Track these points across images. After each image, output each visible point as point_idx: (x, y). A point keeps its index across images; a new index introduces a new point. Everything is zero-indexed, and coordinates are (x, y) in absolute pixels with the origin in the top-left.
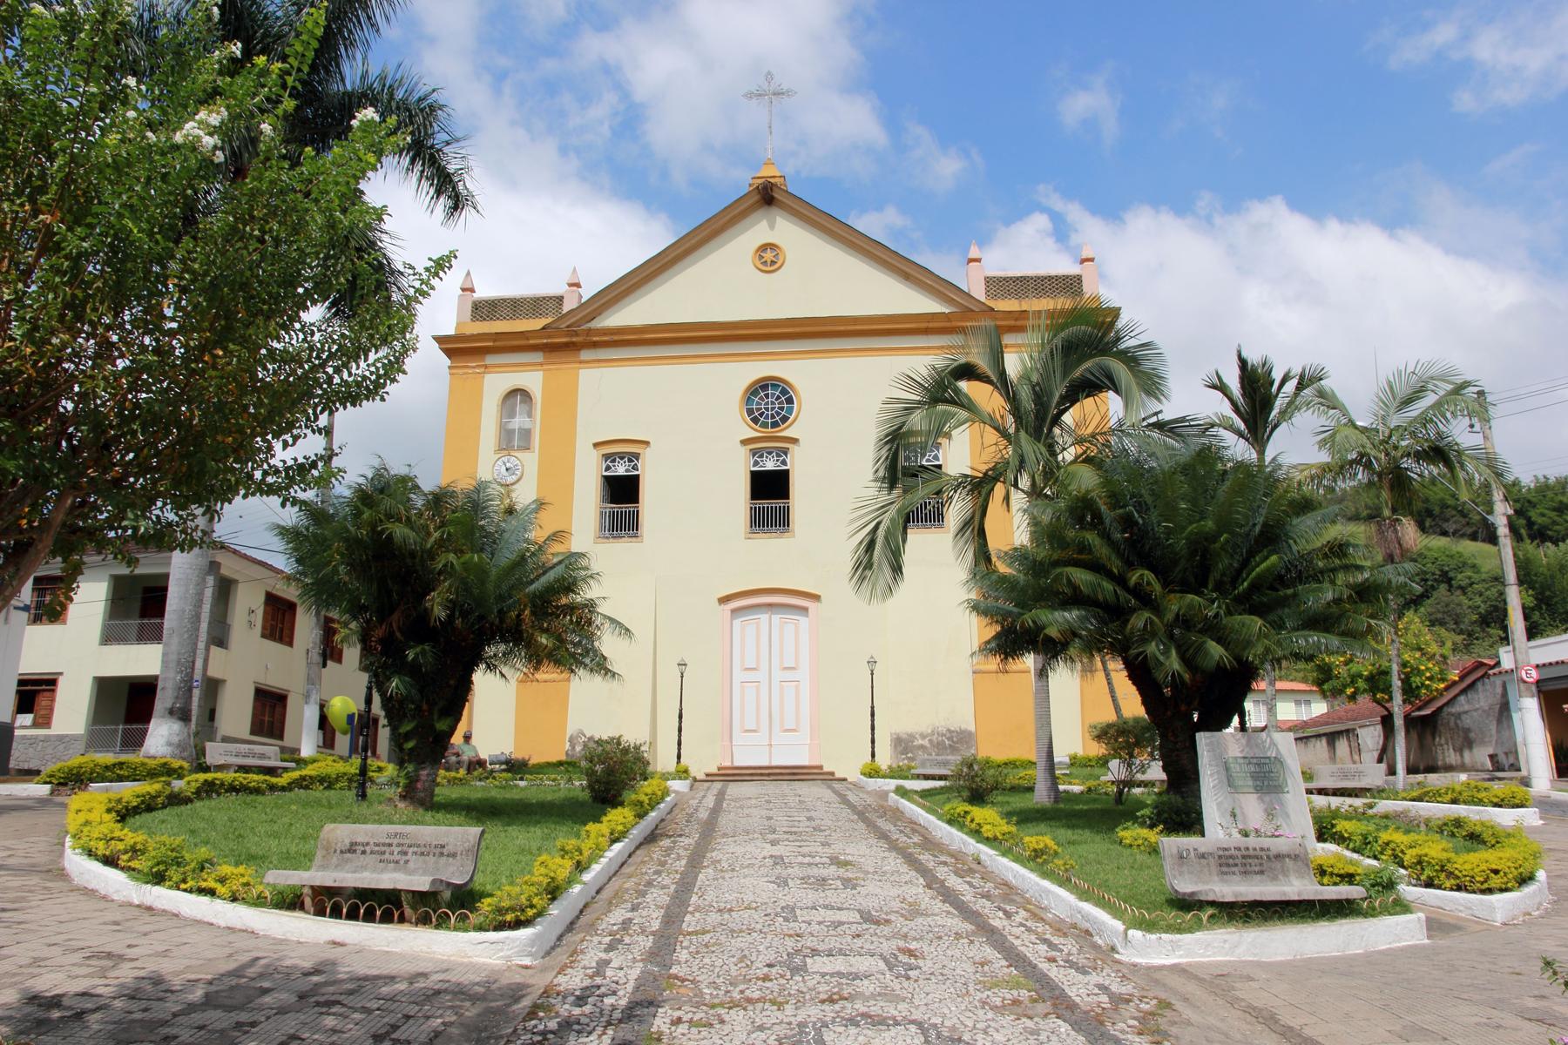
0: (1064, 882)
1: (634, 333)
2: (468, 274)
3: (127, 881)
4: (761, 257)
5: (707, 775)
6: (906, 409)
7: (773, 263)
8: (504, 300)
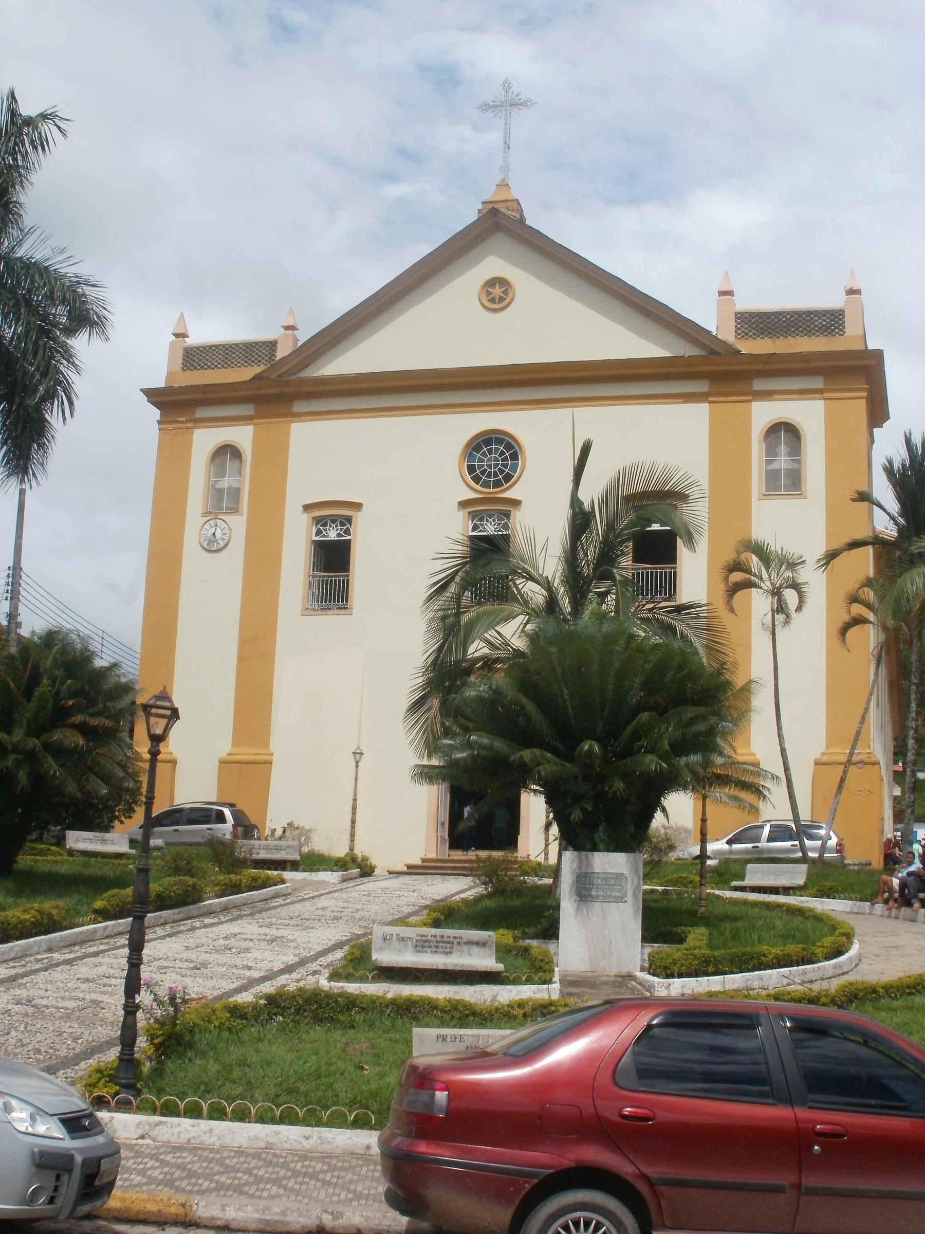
4: (489, 293)
8: (217, 346)
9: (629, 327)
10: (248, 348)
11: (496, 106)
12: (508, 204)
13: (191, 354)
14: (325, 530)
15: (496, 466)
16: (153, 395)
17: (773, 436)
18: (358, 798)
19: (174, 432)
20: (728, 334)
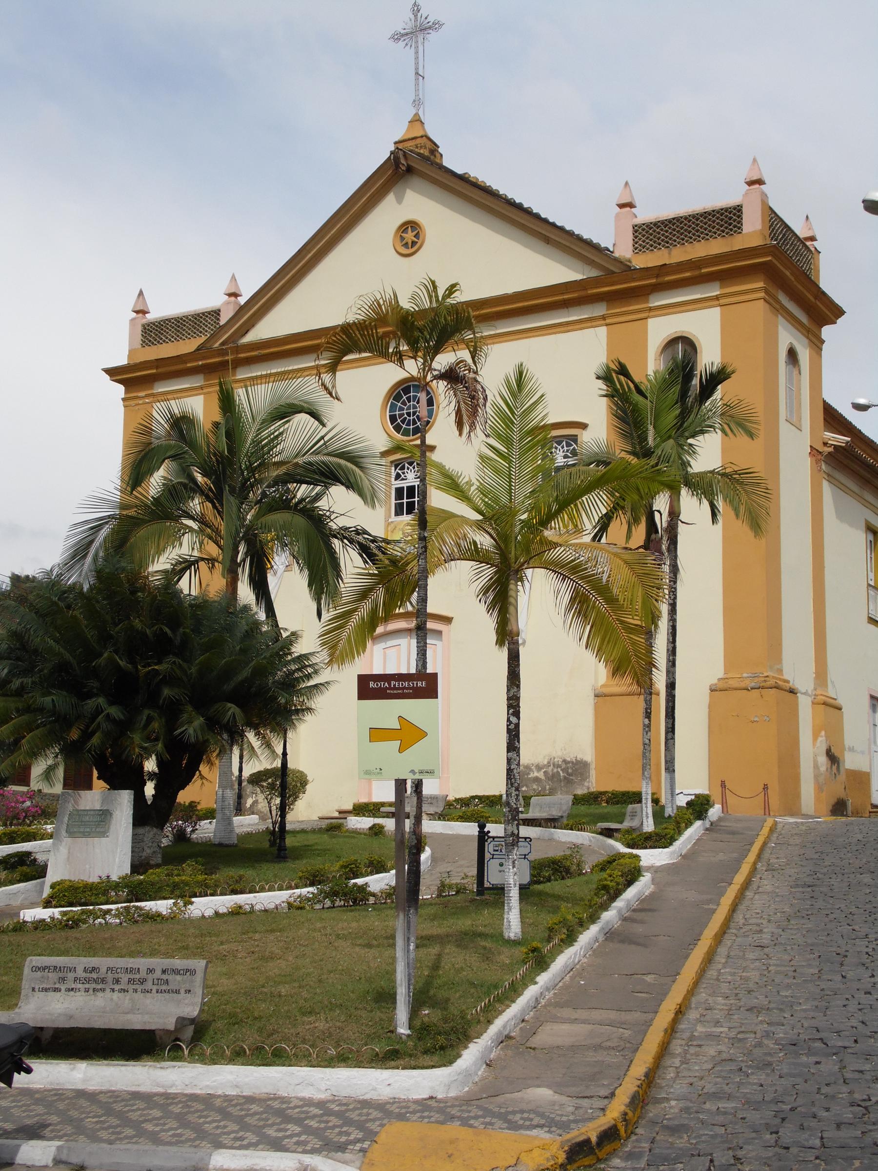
0: (262, 890)
1: (272, 353)
2: (141, 293)
3: (668, 1021)
4: (402, 238)
5: (340, 812)
6: (92, 528)
7: (414, 243)
8: (169, 320)
9: (526, 246)
10: (179, 322)
11: (407, 34)
12: (418, 141)
13: (149, 330)
14: (404, 473)
15: (409, 408)
16: (113, 373)
17: (670, 349)
18: (288, 751)
19: (137, 408)
20: (624, 250)
